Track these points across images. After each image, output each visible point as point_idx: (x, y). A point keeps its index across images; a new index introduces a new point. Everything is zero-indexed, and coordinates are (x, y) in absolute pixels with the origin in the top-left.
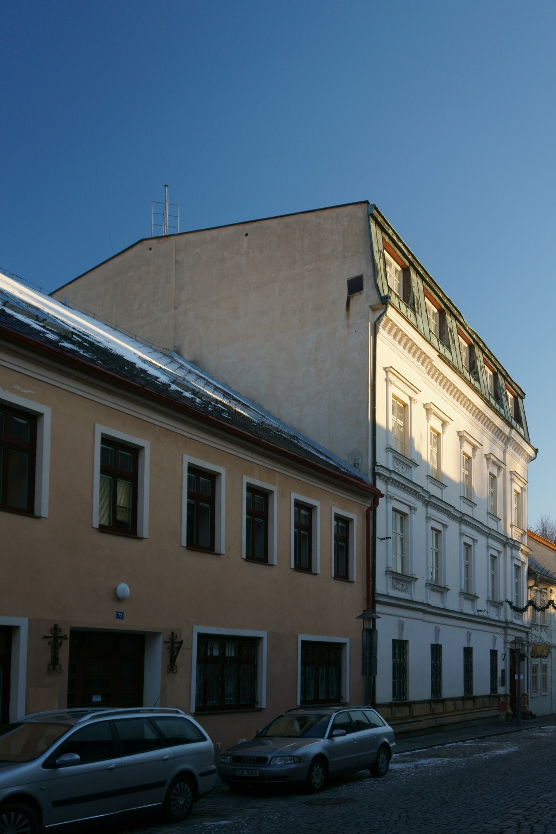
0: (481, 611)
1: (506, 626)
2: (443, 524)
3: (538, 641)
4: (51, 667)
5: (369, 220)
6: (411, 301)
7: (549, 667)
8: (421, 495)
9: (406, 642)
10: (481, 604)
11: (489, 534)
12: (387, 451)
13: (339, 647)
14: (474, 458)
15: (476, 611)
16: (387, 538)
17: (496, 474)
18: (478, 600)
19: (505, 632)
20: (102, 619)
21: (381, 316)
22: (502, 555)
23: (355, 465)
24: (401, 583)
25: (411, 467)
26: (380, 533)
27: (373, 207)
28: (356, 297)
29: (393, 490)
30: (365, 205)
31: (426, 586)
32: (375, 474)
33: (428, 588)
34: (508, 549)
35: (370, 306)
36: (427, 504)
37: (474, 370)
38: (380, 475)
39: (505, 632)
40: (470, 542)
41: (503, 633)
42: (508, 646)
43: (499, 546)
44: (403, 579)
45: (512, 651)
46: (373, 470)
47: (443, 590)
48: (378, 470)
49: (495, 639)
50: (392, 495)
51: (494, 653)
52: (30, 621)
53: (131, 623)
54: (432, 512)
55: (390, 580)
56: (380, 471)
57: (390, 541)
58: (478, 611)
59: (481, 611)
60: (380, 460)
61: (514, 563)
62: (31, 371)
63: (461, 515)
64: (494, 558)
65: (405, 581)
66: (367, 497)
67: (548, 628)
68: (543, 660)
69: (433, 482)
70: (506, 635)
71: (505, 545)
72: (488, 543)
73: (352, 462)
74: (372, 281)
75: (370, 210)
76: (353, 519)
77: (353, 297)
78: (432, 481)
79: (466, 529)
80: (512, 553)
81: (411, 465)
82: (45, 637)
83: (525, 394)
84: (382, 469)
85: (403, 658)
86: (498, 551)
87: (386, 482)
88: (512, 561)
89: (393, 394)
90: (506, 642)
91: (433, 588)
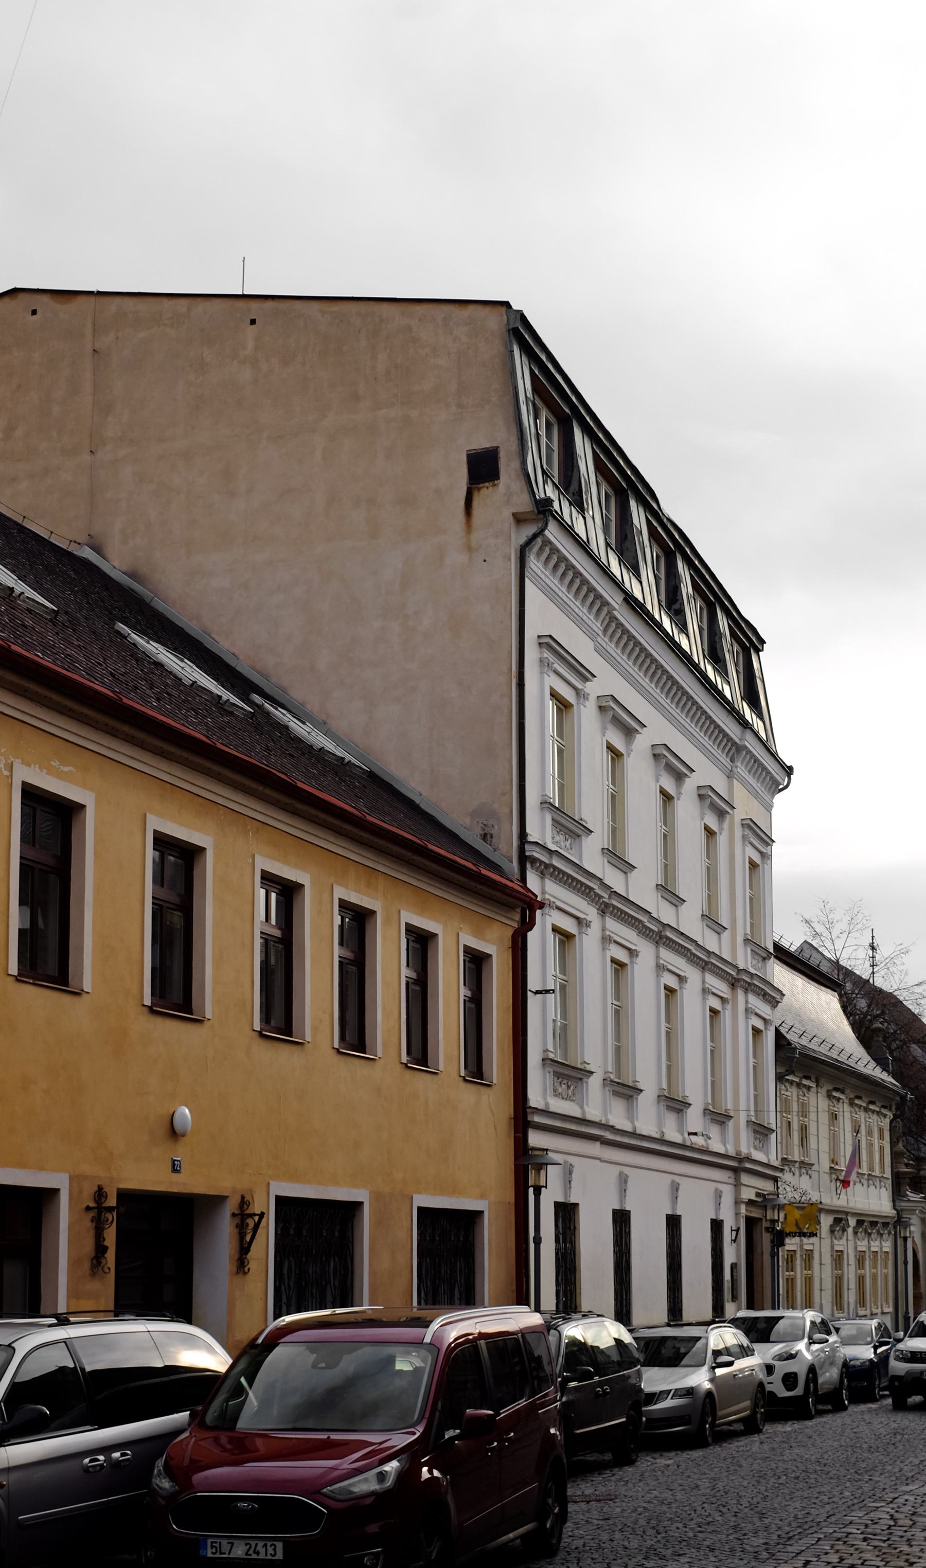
0: (696, 1134)
1: (738, 1167)
2: (629, 949)
3: (798, 1199)
4: (95, 1262)
5: (510, 341)
6: (574, 487)
7: (816, 1255)
8: (596, 894)
9: (576, 1205)
10: (695, 1119)
11: (707, 963)
12: (542, 809)
13: (473, 1217)
14: (678, 799)
15: (686, 1135)
16: (547, 992)
17: (714, 826)
18: (641, 1098)
19: (737, 1179)
20: (150, 1176)
21: (535, 536)
22: (729, 1007)
23: (484, 837)
24: (565, 1081)
25: (579, 836)
26: (533, 983)
27: (518, 316)
28: (484, 492)
29: (552, 891)
30: (504, 309)
31: (604, 1085)
32: (523, 859)
33: (607, 1088)
34: (740, 993)
35: (513, 514)
36: (604, 909)
37: (676, 606)
38: (534, 861)
39: (737, 1179)
40: (622, 956)
41: (732, 1181)
42: (743, 1209)
43: (721, 987)
44: (569, 1075)
45: (751, 1223)
46: (522, 850)
47: (630, 1093)
48: (531, 851)
49: (718, 1195)
50: (552, 899)
51: (717, 1226)
52: (71, 1178)
53: (189, 1182)
54: (614, 926)
55: (549, 1078)
56: (536, 855)
57: (551, 997)
58: (690, 1134)
59: (696, 1134)
60: (533, 833)
61: (609, 954)
62: (8, 705)
63: (661, 928)
64: (714, 1012)
65: (568, 1077)
66: (512, 908)
67: (814, 1168)
68: (805, 1240)
69: (666, 896)
70: (737, 1185)
71: (733, 984)
72: (704, 982)
73: (479, 831)
74: (516, 464)
75: (512, 321)
76: (490, 956)
77: (479, 489)
78: (709, 924)
79: (669, 957)
80: (747, 1002)
81: (580, 832)
82: (88, 1208)
83: (763, 642)
84: (537, 849)
85: (571, 1243)
86: (721, 998)
87: (542, 873)
88: (747, 1018)
89: (551, 688)
90: (737, 1202)
91: (670, 1104)
